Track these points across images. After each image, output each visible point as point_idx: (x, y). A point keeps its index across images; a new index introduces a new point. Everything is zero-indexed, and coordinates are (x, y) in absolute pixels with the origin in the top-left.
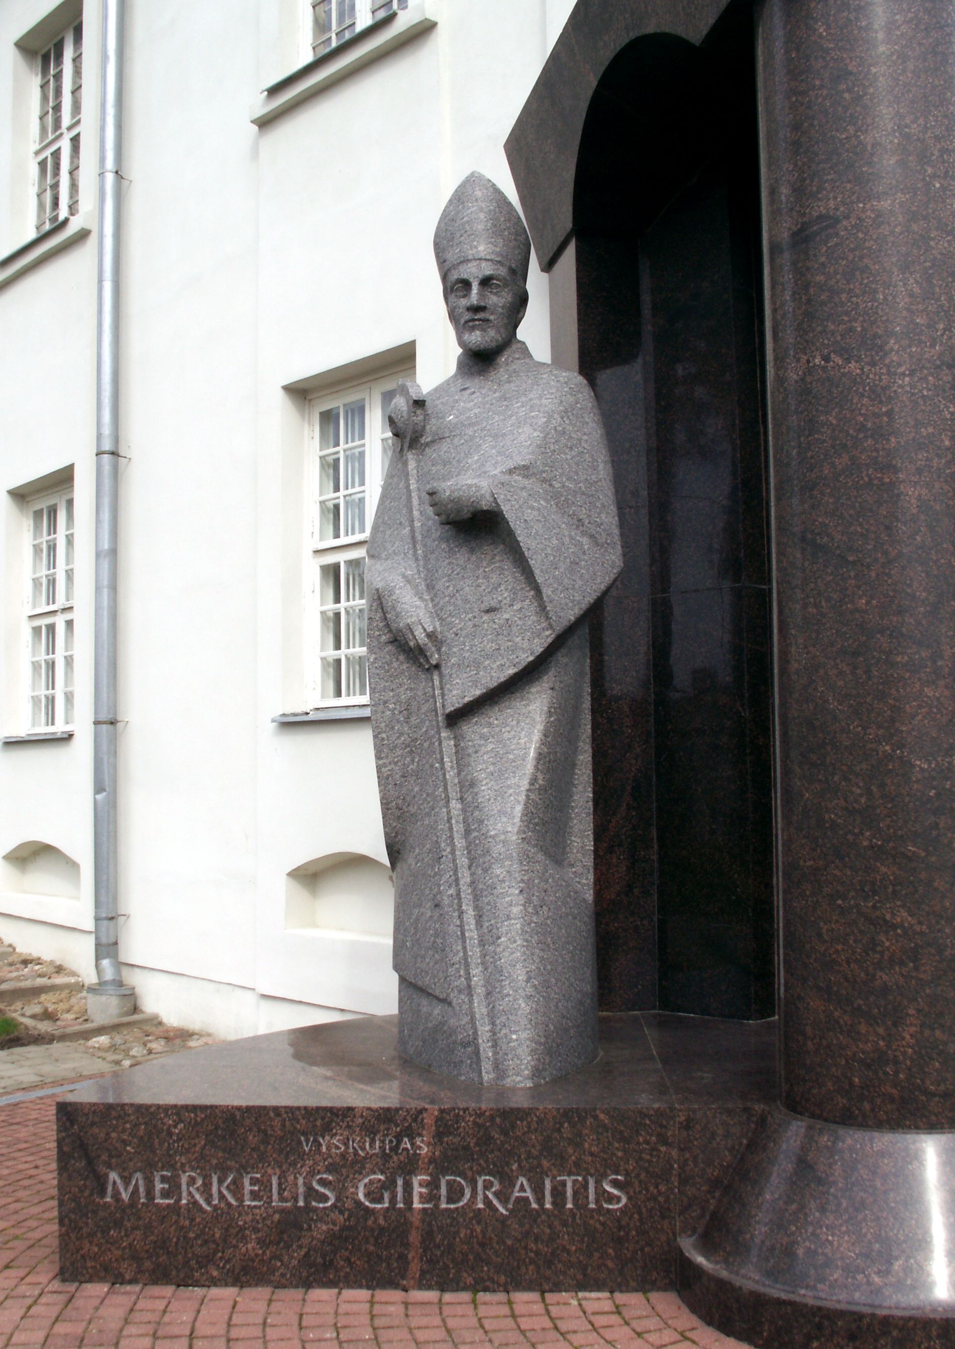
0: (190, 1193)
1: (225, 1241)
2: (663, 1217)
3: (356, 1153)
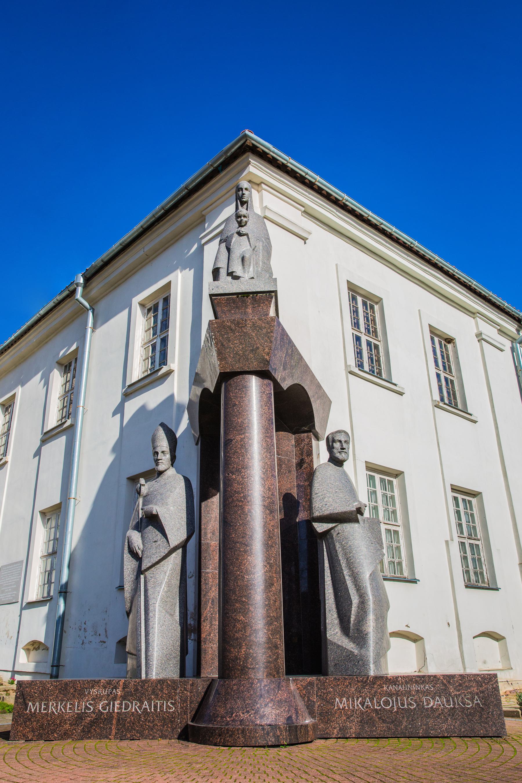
0: (52, 709)
1: (60, 724)
2: (185, 714)
3: (100, 695)
